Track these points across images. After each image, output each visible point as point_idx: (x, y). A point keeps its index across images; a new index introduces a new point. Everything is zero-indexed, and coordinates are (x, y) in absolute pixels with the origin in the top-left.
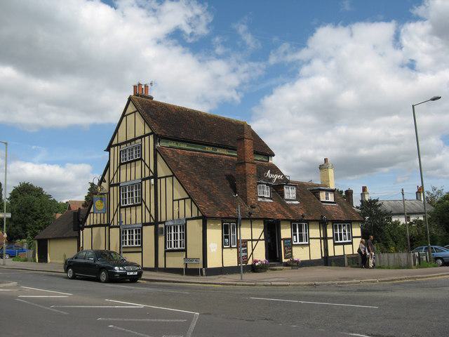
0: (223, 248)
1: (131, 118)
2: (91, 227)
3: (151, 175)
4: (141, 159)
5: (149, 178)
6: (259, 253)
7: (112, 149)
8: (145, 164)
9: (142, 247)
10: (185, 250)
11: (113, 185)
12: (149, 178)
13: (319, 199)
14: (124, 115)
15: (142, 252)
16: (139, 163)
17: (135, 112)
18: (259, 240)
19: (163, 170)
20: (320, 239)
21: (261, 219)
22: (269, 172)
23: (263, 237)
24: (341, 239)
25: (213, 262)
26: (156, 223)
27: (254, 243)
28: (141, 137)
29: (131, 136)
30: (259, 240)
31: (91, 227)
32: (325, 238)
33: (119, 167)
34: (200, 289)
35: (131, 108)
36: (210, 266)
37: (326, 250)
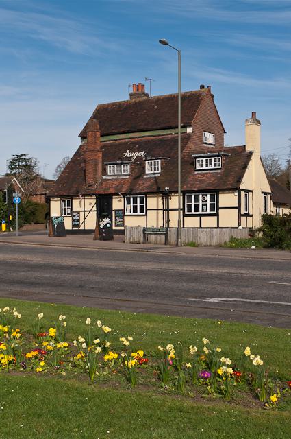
22: (128, 151)
23: (95, 208)
27: (86, 213)
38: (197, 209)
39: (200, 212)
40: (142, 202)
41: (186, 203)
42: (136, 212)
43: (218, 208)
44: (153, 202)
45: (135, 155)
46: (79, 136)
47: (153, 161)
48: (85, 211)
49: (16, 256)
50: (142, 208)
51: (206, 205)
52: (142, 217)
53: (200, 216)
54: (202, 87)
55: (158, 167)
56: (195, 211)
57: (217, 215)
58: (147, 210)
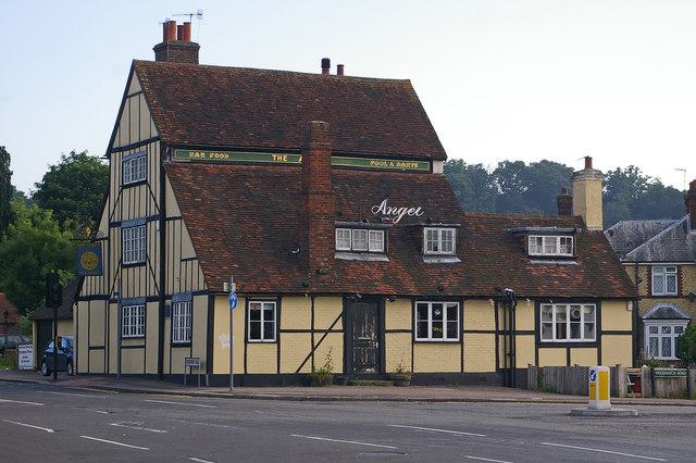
0: (246, 342)
1: (134, 100)
2: (89, 298)
3: (158, 213)
4: (145, 182)
5: (154, 218)
6: (331, 354)
7: (113, 155)
8: (151, 192)
9: (145, 338)
10: (190, 345)
11: (118, 224)
12: (154, 218)
13: (524, 251)
14: (126, 96)
15: (144, 347)
16: (144, 187)
17: (139, 93)
18: (330, 330)
19: (173, 209)
20: (497, 332)
21: (336, 294)
22: (384, 203)
23: (339, 326)
24: (575, 334)
25: (220, 367)
26: (162, 297)
27: (318, 337)
28: (146, 142)
29: (135, 140)
30: (330, 330)
31: (89, 298)
32: (508, 333)
33: (121, 192)
34: (564, 440)
35: (136, 87)
36: (216, 371)
37: (511, 354)
38: (561, 332)
39: (569, 339)
40: (452, 313)
41: (249, 321)
42: (565, 338)
43: (600, 333)
44: (479, 317)
45: (402, 212)
46: (462, 160)
47: (440, 230)
48: (313, 331)
49: (576, 429)
50: (269, 327)
51: (434, 317)
52: (451, 346)
53: (568, 346)
54: (326, 63)
55: (450, 243)
56: (572, 337)
57: (597, 345)
58: (462, 332)
